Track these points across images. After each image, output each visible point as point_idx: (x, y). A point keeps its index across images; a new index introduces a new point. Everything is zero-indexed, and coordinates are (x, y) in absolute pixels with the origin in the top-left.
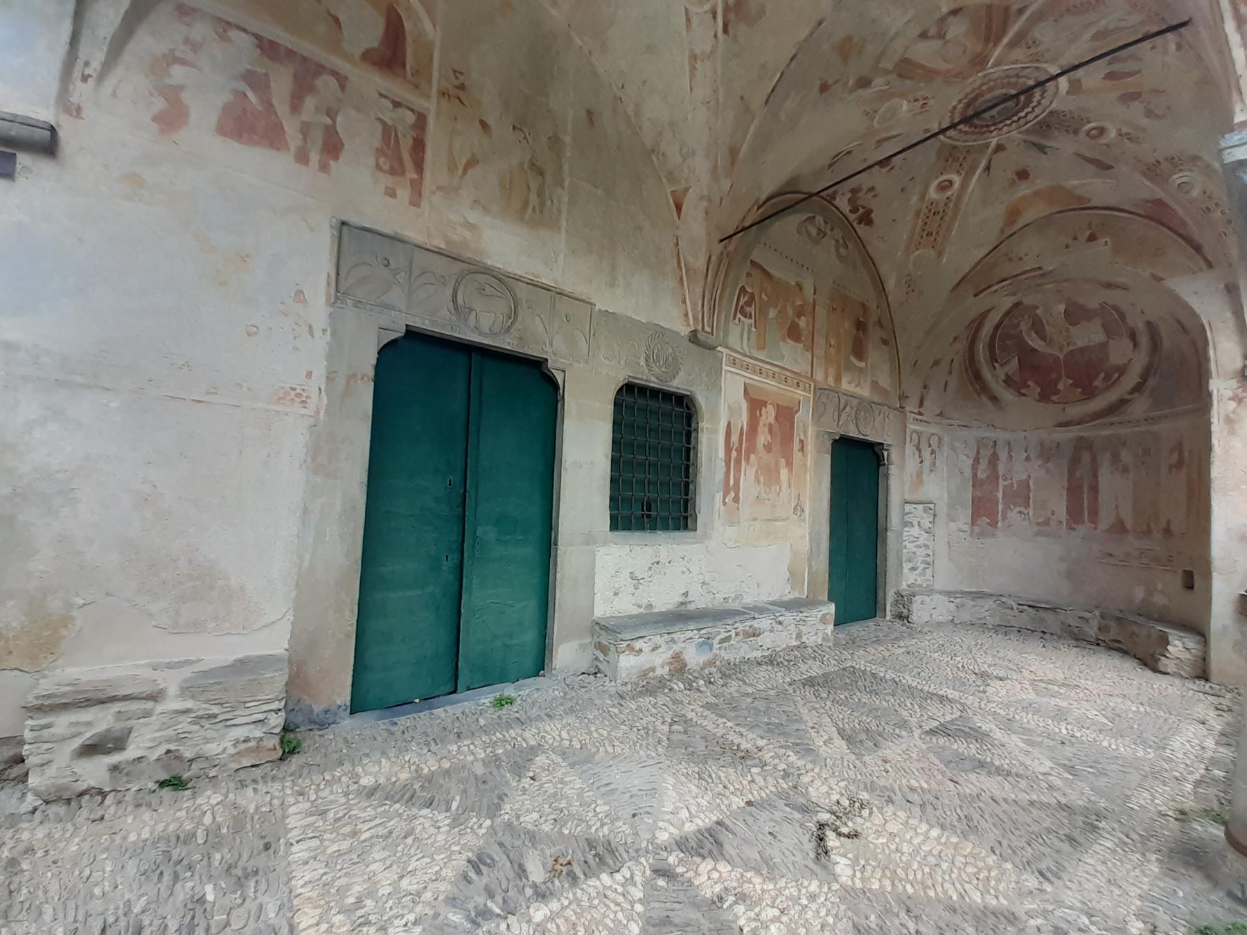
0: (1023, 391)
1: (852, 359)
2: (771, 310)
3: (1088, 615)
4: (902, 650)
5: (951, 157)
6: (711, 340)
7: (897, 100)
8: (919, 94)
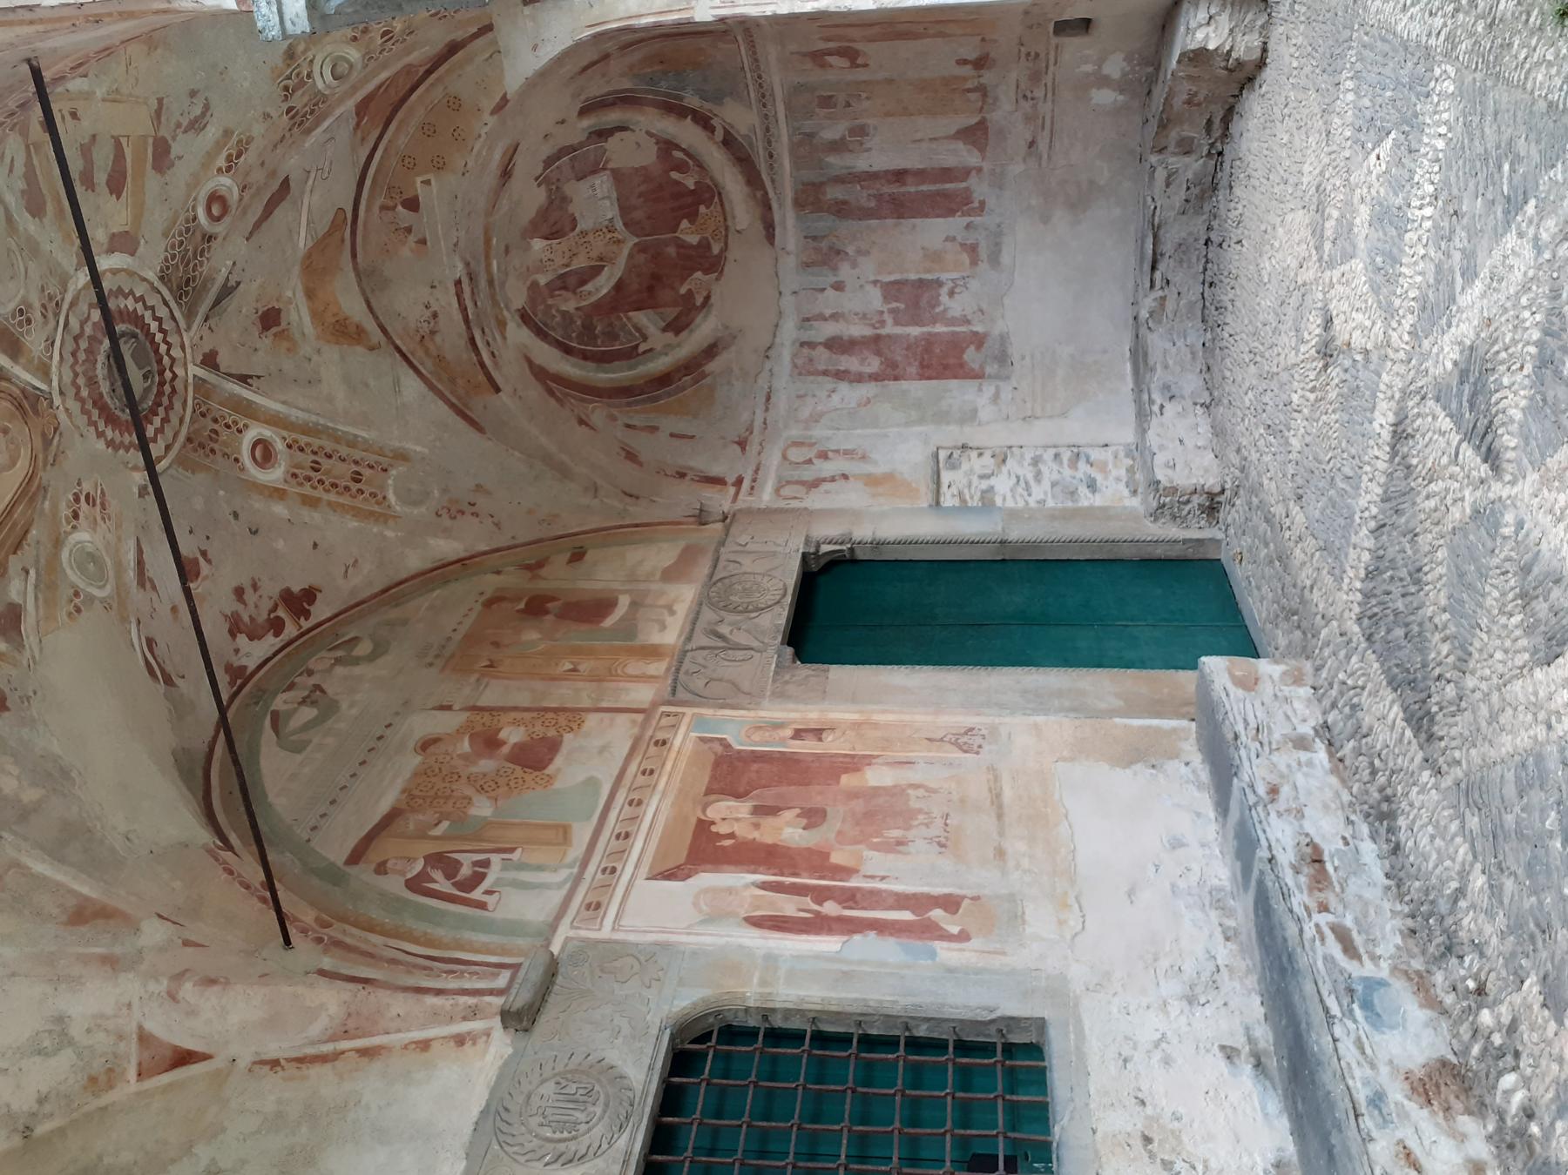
0: (699, 301)
1: (609, 622)
2: (473, 811)
3: (1161, 174)
4: (1295, 510)
5: (205, 445)
6: (532, 974)
7: (65, 555)
8: (65, 512)
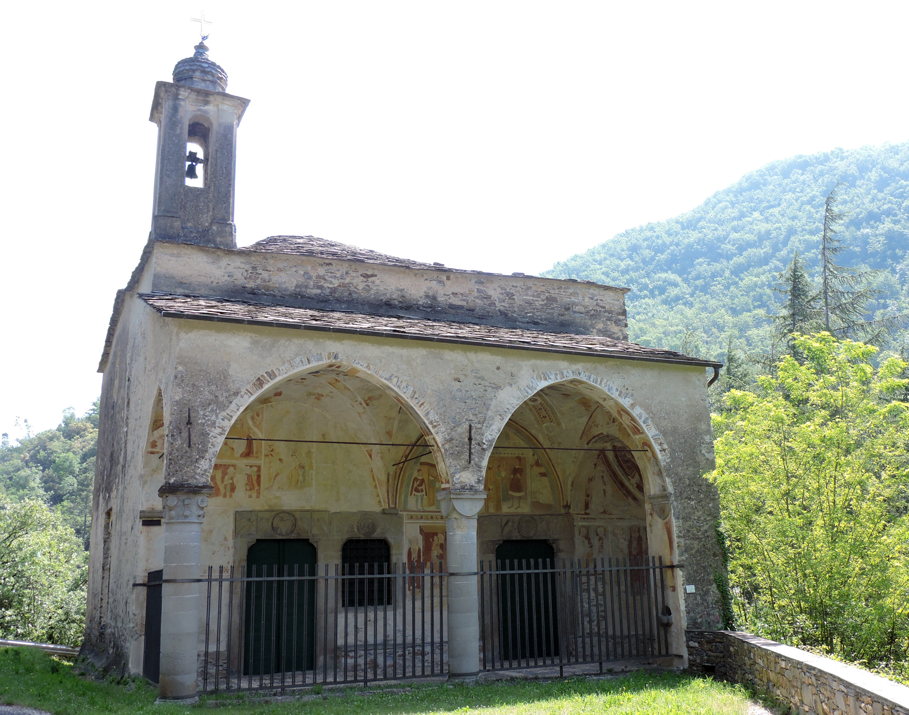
1: (511, 493)
